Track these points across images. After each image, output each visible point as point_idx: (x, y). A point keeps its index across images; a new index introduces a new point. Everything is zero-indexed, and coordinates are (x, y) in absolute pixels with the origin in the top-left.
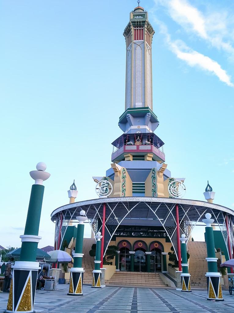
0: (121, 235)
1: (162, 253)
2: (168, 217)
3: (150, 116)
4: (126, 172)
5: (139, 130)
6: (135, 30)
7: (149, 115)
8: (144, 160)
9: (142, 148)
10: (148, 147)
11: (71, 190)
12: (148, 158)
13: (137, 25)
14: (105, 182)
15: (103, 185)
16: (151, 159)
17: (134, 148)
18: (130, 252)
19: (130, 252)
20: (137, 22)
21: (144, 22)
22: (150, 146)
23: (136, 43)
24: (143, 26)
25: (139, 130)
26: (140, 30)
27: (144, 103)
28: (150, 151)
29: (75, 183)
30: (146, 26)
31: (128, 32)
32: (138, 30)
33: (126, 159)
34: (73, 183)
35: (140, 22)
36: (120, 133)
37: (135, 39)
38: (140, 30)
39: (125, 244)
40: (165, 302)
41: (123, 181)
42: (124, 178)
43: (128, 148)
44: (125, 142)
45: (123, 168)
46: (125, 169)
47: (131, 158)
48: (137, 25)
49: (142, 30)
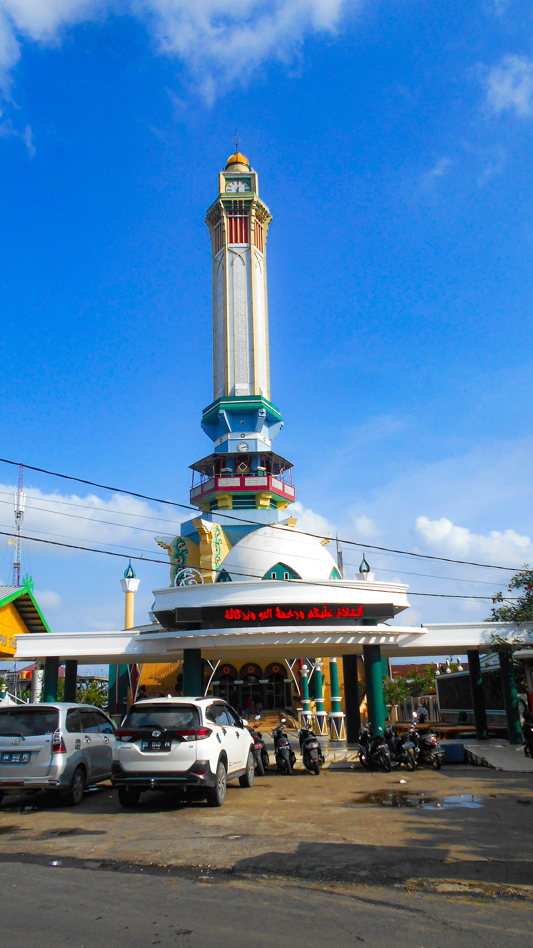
0: (298, 709)
1: (285, 680)
2: (286, 634)
3: (264, 415)
4: (221, 532)
5: (244, 441)
6: (230, 219)
7: (263, 413)
8: (255, 508)
9: (250, 482)
10: (262, 481)
11: (127, 580)
12: (262, 502)
13: (235, 207)
14: (191, 572)
15: (187, 577)
16: (268, 503)
17: (236, 482)
18: (236, 682)
19: (236, 682)
20: (235, 202)
21: (251, 202)
22: (266, 478)
23: (234, 250)
24: (247, 211)
25: (244, 441)
26: (241, 218)
27: (252, 383)
28: (265, 488)
29: (132, 566)
30: (253, 212)
31: (215, 219)
32: (236, 219)
33: (219, 505)
34: (128, 565)
35: (241, 202)
36: (206, 448)
37: (231, 242)
38: (241, 218)
39: (226, 670)
40: (359, 899)
41: (217, 550)
42: (218, 544)
43: (223, 482)
44: (218, 471)
45: (216, 524)
46: (220, 528)
47: (230, 503)
48: (235, 207)
49: (246, 218)
